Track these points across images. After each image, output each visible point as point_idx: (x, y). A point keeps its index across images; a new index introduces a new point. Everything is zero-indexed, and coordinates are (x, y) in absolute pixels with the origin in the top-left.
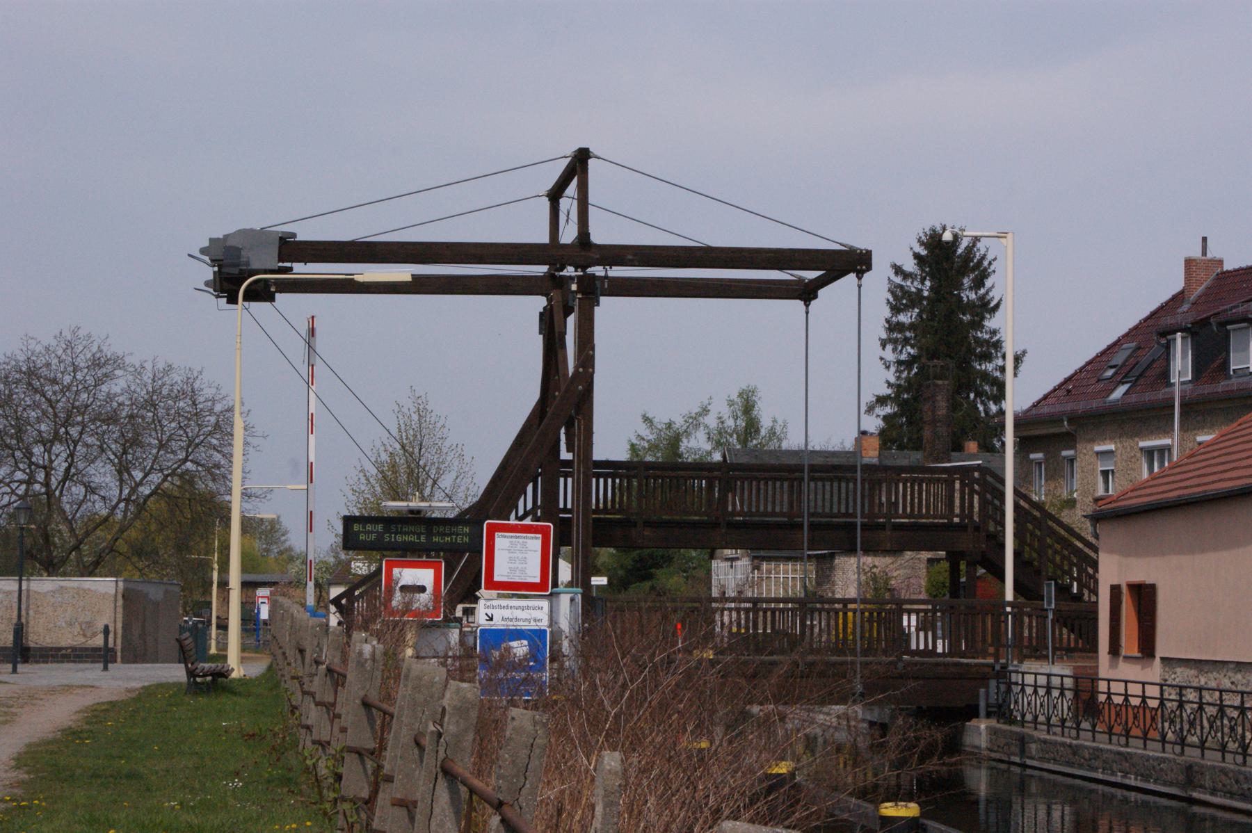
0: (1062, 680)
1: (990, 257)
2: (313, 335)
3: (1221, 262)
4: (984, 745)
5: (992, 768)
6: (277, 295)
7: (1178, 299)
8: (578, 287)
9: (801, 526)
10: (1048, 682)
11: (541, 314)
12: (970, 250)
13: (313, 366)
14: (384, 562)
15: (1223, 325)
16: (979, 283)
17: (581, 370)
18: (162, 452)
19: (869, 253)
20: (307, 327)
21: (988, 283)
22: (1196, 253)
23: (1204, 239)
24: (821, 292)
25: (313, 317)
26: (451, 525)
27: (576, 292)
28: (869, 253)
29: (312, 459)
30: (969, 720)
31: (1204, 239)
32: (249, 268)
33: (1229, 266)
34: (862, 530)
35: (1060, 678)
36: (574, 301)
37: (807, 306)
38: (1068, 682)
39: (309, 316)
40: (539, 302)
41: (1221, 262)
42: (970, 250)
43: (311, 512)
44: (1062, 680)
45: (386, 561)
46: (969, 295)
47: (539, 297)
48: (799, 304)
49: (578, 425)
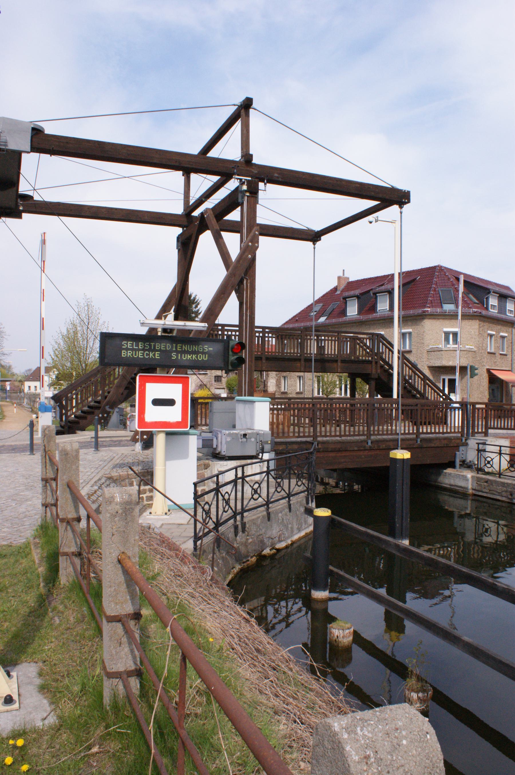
0: (500, 448)
1: (200, 300)
2: (44, 244)
3: (348, 278)
4: (470, 487)
5: (472, 500)
6: (24, 215)
7: (335, 289)
8: (248, 188)
9: (311, 360)
10: (500, 451)
11: (178, 238)
12: (195, 298)
13: (44, 261)
14: (138, 378)
15: (375, 294)
16: (196, 307)
17: (250, 244)
18: (376, 719)
19: (409, 192)
20: (40, 239)
21: (199, 307)
22: (341, 275)
23: (344, 270)
24: (322, 238)
25: (44, 233)
26: (182, 344)
27: (246, 191)
28: (409, 192)
29: (43, 316)
30: (445, 469)
31: (344, 270)
32: (7, 148)
33: (351, 280)
34: (315, 361)
35: (499, 447)
36: (243, 198)
37: (314, 244)
38: (507, 451)
39: (42, 232)
40: (179, 231)
41: (348, 278)
42: (195, 298)
43: (43, 347)
44: (500, 448)
45: (140, 376)
46: (194, 310)
47: (177, 228)
48: (310, 244)
49: (246, 283)
